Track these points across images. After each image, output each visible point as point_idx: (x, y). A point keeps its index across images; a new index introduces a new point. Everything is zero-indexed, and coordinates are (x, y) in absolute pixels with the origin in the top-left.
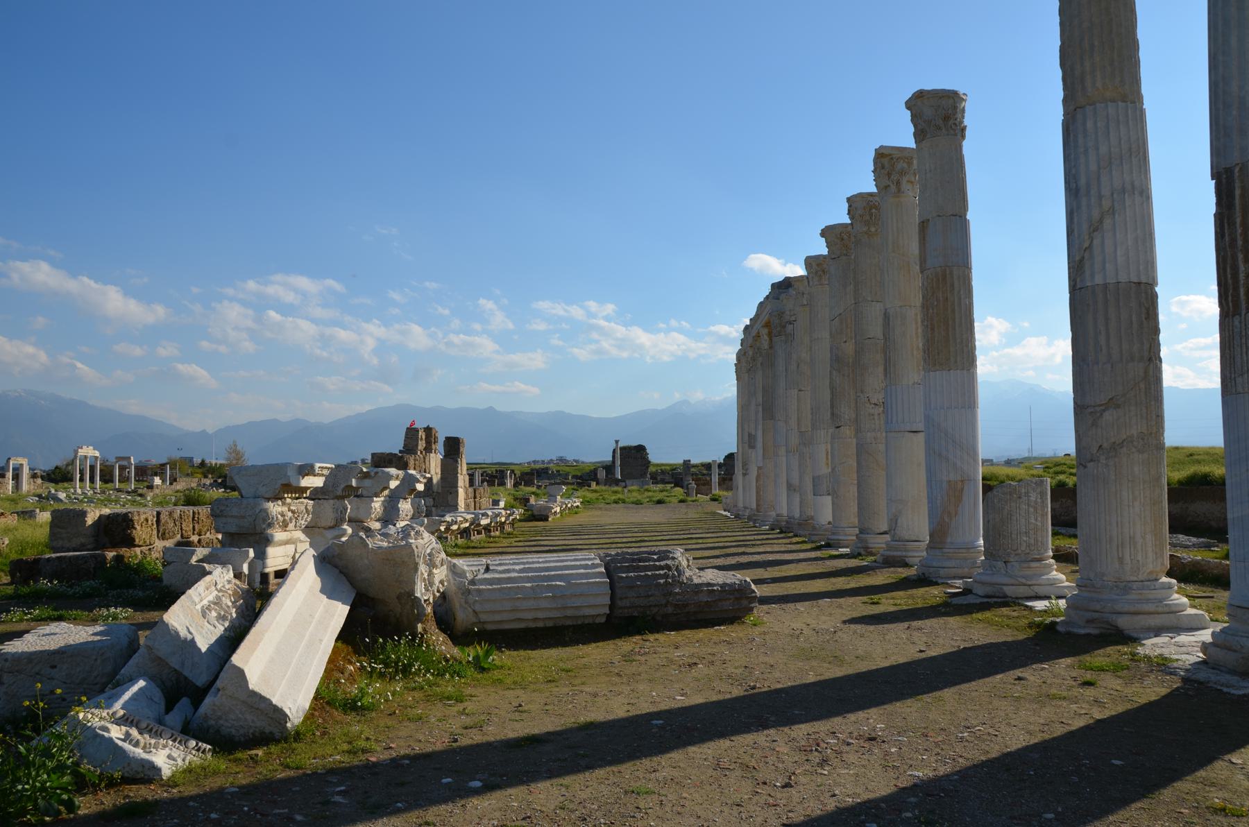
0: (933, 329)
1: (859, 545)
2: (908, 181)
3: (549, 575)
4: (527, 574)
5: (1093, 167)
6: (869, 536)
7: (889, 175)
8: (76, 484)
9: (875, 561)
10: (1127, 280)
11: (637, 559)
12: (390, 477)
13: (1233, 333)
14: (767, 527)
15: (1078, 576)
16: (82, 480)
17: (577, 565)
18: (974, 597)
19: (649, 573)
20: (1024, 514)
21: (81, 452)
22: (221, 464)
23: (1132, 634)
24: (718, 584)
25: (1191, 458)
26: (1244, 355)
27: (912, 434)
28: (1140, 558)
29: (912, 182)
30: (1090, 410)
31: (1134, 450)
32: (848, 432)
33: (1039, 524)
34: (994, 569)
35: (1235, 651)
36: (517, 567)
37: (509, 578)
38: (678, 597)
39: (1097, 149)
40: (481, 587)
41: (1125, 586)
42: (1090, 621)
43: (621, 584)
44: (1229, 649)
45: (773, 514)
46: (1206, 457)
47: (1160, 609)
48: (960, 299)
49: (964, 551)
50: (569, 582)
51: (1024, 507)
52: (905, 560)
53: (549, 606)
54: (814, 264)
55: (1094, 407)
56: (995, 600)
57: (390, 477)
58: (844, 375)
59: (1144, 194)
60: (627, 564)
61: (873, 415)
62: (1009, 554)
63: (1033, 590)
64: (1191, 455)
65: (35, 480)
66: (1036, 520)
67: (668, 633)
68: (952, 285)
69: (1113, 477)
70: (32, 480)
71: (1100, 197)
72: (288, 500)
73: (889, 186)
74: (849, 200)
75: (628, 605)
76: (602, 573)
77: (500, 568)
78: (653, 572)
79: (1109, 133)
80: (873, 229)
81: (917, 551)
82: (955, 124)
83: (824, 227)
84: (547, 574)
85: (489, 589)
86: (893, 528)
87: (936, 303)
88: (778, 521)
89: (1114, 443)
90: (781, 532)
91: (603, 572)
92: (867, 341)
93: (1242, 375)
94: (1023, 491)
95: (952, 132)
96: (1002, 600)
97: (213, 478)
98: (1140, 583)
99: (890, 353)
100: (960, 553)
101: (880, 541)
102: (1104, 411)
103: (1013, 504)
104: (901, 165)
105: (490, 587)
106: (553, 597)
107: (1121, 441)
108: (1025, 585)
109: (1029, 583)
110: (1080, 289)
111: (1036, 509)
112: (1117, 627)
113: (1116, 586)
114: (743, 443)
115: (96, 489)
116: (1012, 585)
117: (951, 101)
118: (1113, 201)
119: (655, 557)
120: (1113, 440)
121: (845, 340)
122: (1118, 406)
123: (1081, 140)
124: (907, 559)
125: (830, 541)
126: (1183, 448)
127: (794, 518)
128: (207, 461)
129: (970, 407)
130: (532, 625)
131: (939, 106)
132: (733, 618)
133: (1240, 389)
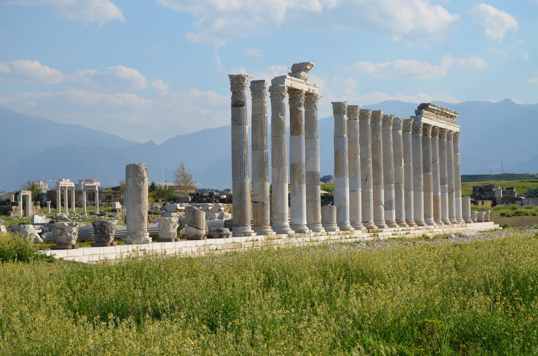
8: (73, 208)
12: (209, 206)
21: (62, 184)
22: (170, 187)
57: (209, 206)
65: (37, 207)
68: (339, 155)
72: (178, 212)
97: (162, 201)
128: (157, 184)
129: (343, 187)
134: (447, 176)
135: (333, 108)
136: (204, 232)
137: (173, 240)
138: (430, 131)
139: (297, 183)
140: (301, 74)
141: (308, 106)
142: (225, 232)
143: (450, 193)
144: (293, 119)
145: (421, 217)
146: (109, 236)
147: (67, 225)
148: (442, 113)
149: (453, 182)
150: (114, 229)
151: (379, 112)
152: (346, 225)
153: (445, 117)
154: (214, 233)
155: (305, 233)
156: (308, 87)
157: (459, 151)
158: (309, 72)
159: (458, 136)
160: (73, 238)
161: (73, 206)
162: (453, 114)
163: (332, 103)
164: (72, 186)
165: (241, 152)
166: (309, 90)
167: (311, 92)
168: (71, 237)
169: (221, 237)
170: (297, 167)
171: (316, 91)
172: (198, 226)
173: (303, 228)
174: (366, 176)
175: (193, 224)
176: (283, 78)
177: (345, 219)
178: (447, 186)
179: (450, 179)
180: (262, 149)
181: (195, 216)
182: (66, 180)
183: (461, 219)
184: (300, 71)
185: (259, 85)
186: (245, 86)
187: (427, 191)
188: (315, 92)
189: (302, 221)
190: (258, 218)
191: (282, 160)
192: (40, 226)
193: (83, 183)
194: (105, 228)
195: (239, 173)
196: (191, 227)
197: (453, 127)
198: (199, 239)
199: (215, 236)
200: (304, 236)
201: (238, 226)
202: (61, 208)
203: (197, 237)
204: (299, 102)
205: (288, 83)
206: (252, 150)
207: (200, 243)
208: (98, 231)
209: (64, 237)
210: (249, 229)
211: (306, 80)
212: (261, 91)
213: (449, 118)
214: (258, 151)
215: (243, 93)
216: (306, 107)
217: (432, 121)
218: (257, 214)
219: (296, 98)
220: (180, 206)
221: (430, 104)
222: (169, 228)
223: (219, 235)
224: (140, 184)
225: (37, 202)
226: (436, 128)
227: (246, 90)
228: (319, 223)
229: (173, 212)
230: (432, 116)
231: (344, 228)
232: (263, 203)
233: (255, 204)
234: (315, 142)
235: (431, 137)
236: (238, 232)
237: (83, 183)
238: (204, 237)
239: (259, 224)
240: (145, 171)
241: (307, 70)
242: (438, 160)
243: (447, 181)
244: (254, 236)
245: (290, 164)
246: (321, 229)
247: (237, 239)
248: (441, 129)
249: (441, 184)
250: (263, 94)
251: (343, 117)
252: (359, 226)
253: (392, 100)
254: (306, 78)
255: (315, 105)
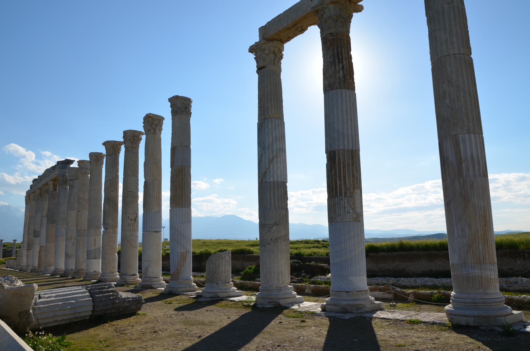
0: (176, 191)
1: (122, 281)
2: (158, 129)
3: (68, 298)
4: (64, 297)
5: (271, 140)
6: (127, 276)
7: (151, 125)
9: (136, 287)
10: (281, 181)
11: (100, 288)
13: (335, 203)
14: (49, 275)
15: (226, 287)
17: (78, 292)
18: (204, 298)
19: (107, 294)
20: (224, 265)
23: (285, 306)
24: (131, 298)
25: (204, 244)
26: (339, 210)
27: (155, 233)
28: (284, 279)
29: (160, 130)
30: (267, 226)
31: (282, 240)
32: (111, 231)
33: (229, 268)
34: (212, 287)
35: (338, 306)
36: (54, 295)
37: (52, 301)
38: (117, 304)
39: (272, 134)
40: (40, 306)
41: (280, 289)
42: (270, 303)
43: (97, 300)
44: (336, 305)
45: (53, 268)
46: (210, 244)
47: (291, 296)
48: (187, 179)
49: (187, 281)
50: (77, 300)
51: (224, 262)
52: (152, 286)
53: (69, 313)
54: (94, 157)
55: (269, 225)
56: (215, 299)
58: (110, 206)
59: (284, 151)
60: (98, 291)
61: (130, 224)
62: (218, 280)
63: (228, 294)
64: (204, 243)
66: (228, 267)
67: (117, 321)
68: (185, 174)
69: (276, 250)
71: (273, 151)
73: (150, 130)
74: (124, 132)
75: (100, 310)
76: (88, 295)
77: (46, 296)
78: (108, 294)
79: (276, 129)
80: (134, 146)
81: (156, 282)
82: (188, 111)
83: (105, 141)
84: (67, 297)
85: (43, 307)
86: (145, 273)
87: (178, 180)
88: (56, 272)
89: (276, 238)
90: (61, 277)
91: (89, 295)
92: (129, 192)
93: (338, 216)
94: (224, 256)
95: (187, 114)
96: (218, 299)
98: (484, 278)
99: (147, 198)
100: (185, 282)
101: (131, 279)
102: (273, 226)
103: (220, 261)
104: (156, 122)
105: (44, 306)
106: (71, 308)
107: (278, 237)
108: (225, 292)
109: (227, 291)
110: (264, 182)
111: (228, 263)
112: (279, 304)
113: (277, 289)
114: (28, 234)
116: (221, 292)
117: (188, 102)
118: (277, 153)
119: (107, 287)
120: (276, 237)
121: (112, 191)
122: (277, 225)
123: (267, 130)
124: (152, 286)
125: (101, 280)
126: (201, 240)
127: (68, 270)
130: (60, 323)
131: (183, 103)
132: (133, 313)
133: (338, 221)
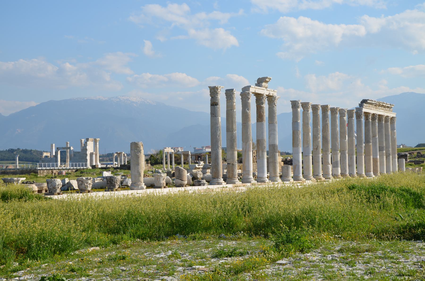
16: (166, 163)
21: (166, 150)
65: (148, 165)
70: (147, 165)
115: (173, 168)
134: (384, 145)
135: (291, 104)
136: (186, 182)
137: (162, 187)
138: (370, 117)
139: (260, 151)
140: (263, 84)
141: (270, 103)
142: (202, 182)
143: (388, 156)
144: (258, 112)
145: (362, 172)
146: (115, 185)
147: (85, 179)
148: (378, 105)
149: (390, 149)
150: (118, 181)
151: (327, 106)
152: (299, 177)
153: (383, 108)
154: (196, 183)
155: (265, 182)
156: (269, 92)
157: (396, 129)
158: (269, 82)
159: (395, 119)
160: (89, 186)
161: (164, 164)
162: (389, 106)
163: (291, 101)
164: (172, 152)
165: (216, 133)
166: (269, 93)
167: (271, 95)
168: (87, 186)
169: (200, 185)
170: (260, 142)
171: (275, 94)
172: (182, 178)
173: (265, 179)
174: (317, 146)
175: (179, 177)
176: (249, 87)
177: (299, 174)
178: (384, 152)
179: (387, 147)
180: (232, 131)
181: (180, 172)
182: (168, 148)
183: (237, 179)
184: (262, 82)
185: (230, 92)
186: (218, 93)
187: (367, 155)
188: (274, 95)
189: (264, 175)
190: (230, 173)
191: (248, 138)
192: (100, 178)
193: (204, 148)
194: (112, 180)
195: (215, 146)
196: (178, 180)
197: (390, 114)
198: (183, 187)
199: (196, 185)
200: (264, 184)
201: (215, 178)
202: (175, 165)
203: (181, 185)
204: (262, 101)
205: (252, 90)
206: (227, 132)
207: (182, 189)
208: (109, 182)
209: (83, 186)
210: (222, 180)
211: (266, 88)
212: (232, 96)
213: (386, 108)
214: (230, 133)
215: (217, 97)
216: (269, 104)
217: (372, 111)
218: (229, 171)
219: (260, 99)
220: (198, 165)
221: (368, 100)
222: (160, 180)
223: (199, 184)
224: (138, 154)
225: (148, 162)
226: (376, 114)
227: (219, 96)
228: (277, 176)
229: (194, 169)
230: (371, 107)
231: (299, 179)
232: (233, 164)
233: (228, 165)
234: (274, 126)
235: (371, 121)
236: (214, 182)
237: (204, 148)
238: (186, 186)
239: (231, 177)
240: (141, 146)
241: (267, 82)
242: (377, 135)
243: (385, 149)
244: (224, 184)
245: (257, 140)
246: (278, 180)
247: (211, 187)
248: (379, 115)
249: (379, 151)
250: (233, 98)
251: (297, 110)
252: (310, 178)
253: (408, 92)
254: (266, 86)
255: (274, 103)
